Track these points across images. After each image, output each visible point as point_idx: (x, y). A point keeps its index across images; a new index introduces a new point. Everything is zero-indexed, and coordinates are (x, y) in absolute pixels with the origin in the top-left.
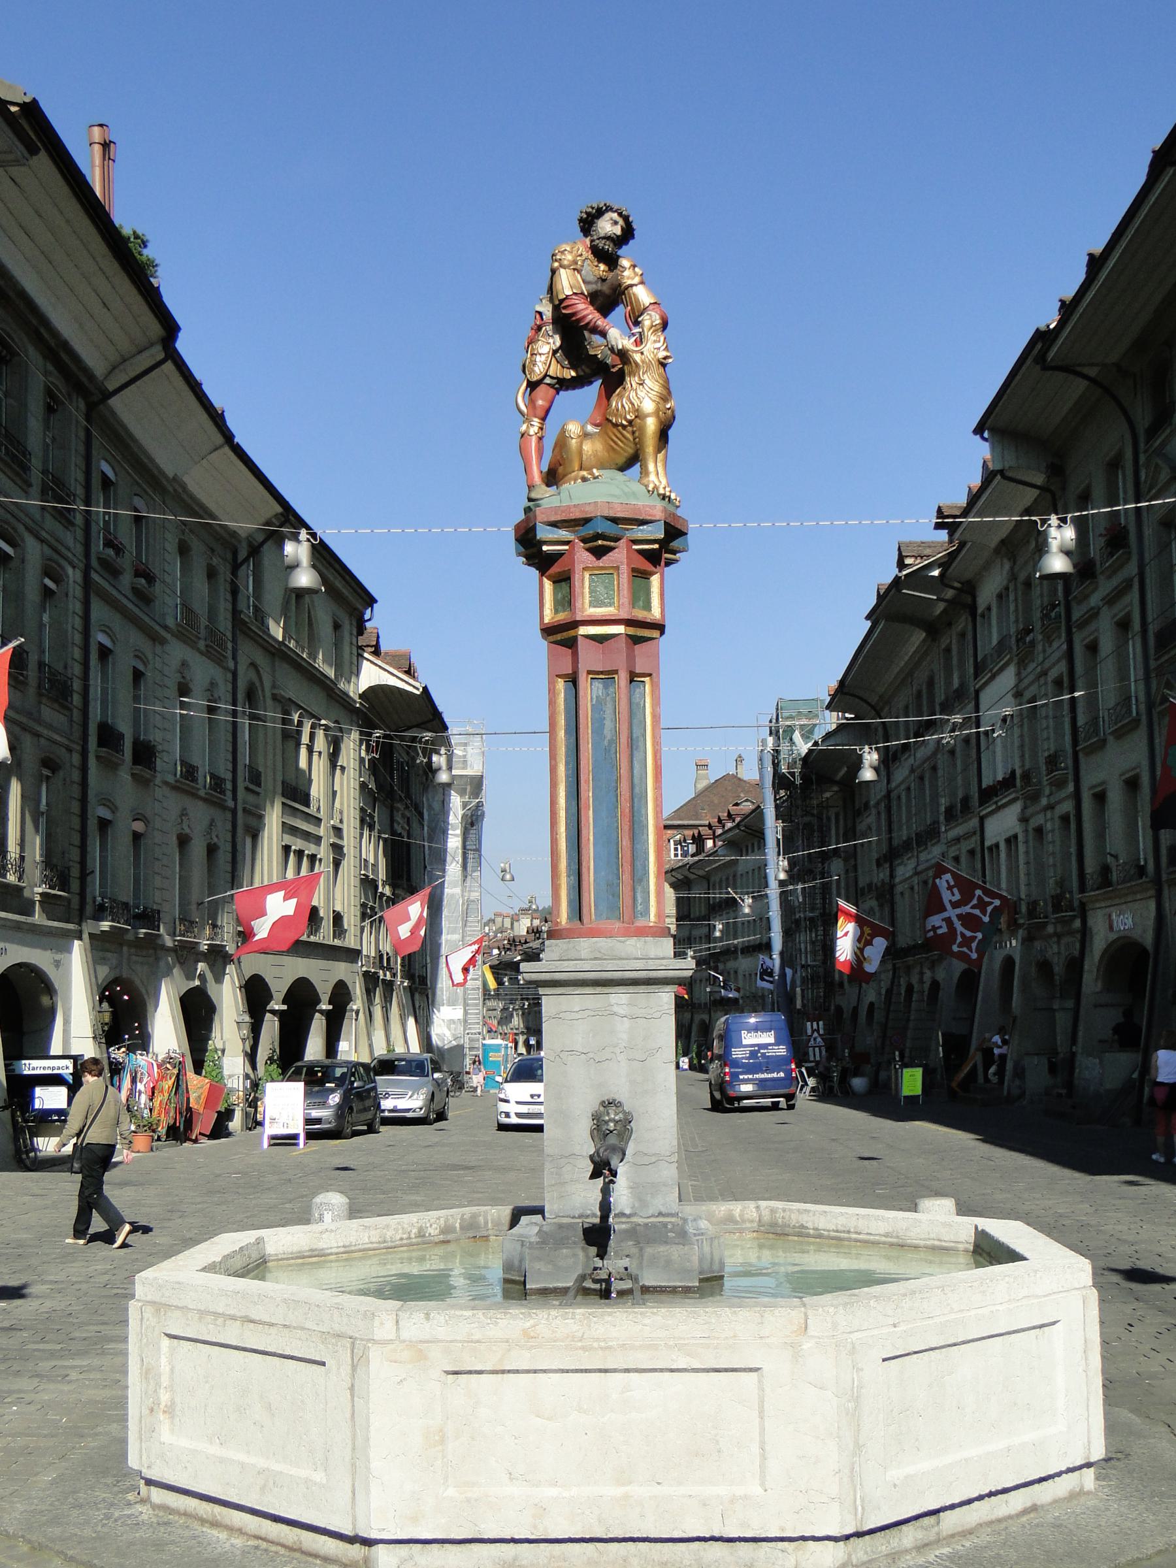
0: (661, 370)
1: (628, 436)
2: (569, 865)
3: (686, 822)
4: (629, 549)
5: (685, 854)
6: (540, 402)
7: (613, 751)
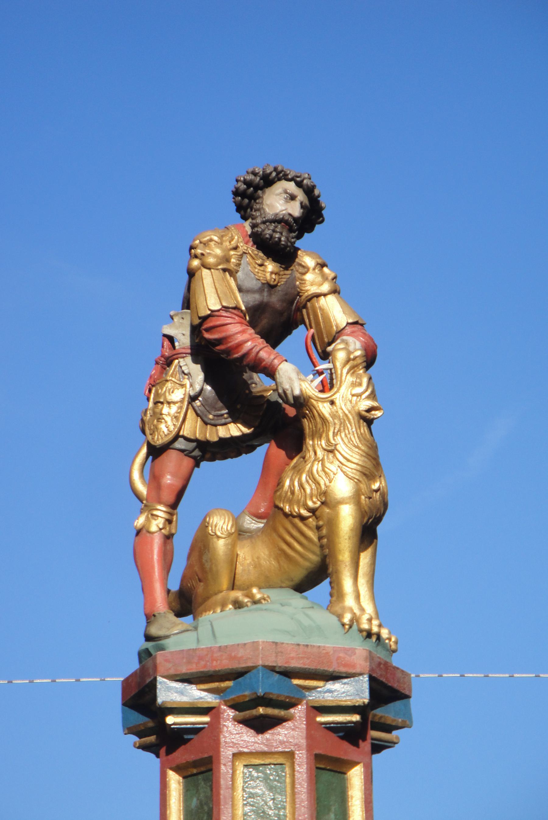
0: (364, 429)
4: (310, 723)
6: (168, 479)
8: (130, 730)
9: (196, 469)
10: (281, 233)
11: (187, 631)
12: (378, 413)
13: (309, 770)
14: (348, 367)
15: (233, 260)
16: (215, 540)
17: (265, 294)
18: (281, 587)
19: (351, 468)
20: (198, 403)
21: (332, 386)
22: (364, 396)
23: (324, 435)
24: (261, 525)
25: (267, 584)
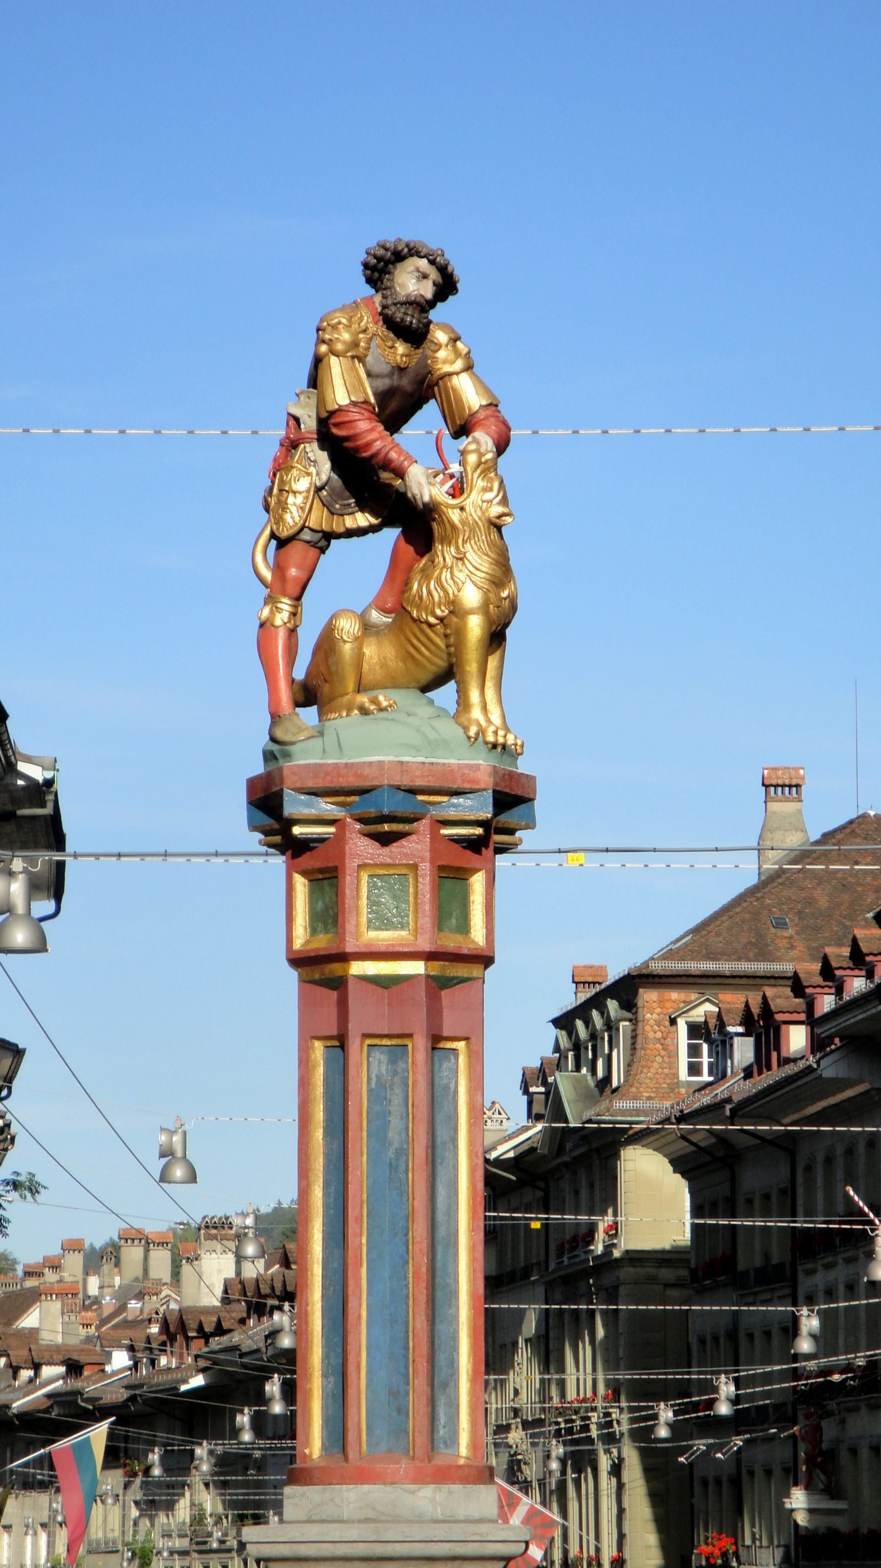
0: (494, 535)
1: (438, 640)
2: (326, 1357)
3: (726, 967)
4: (435, 837)
5: (719, 1073)
6: (293, 572)
7: (402, 1167)
8: (254, 828)
9: (322, 555)
10: (413, 316)
11: (313, 737)
12: (508, 519)
13: (433, 881)
14: (479, 471)
15: (362, 344)
16: (341, 644)
17: (396, 377)
18: (408, 688)
19: (480, 577)
20: (324, 493)
21: (462, 491)
22: (495, 502)
23: (453, 541)
24: (390, 620)
25: (393, 683)
